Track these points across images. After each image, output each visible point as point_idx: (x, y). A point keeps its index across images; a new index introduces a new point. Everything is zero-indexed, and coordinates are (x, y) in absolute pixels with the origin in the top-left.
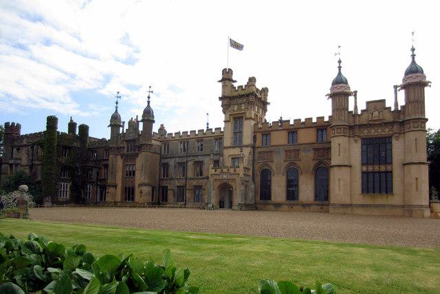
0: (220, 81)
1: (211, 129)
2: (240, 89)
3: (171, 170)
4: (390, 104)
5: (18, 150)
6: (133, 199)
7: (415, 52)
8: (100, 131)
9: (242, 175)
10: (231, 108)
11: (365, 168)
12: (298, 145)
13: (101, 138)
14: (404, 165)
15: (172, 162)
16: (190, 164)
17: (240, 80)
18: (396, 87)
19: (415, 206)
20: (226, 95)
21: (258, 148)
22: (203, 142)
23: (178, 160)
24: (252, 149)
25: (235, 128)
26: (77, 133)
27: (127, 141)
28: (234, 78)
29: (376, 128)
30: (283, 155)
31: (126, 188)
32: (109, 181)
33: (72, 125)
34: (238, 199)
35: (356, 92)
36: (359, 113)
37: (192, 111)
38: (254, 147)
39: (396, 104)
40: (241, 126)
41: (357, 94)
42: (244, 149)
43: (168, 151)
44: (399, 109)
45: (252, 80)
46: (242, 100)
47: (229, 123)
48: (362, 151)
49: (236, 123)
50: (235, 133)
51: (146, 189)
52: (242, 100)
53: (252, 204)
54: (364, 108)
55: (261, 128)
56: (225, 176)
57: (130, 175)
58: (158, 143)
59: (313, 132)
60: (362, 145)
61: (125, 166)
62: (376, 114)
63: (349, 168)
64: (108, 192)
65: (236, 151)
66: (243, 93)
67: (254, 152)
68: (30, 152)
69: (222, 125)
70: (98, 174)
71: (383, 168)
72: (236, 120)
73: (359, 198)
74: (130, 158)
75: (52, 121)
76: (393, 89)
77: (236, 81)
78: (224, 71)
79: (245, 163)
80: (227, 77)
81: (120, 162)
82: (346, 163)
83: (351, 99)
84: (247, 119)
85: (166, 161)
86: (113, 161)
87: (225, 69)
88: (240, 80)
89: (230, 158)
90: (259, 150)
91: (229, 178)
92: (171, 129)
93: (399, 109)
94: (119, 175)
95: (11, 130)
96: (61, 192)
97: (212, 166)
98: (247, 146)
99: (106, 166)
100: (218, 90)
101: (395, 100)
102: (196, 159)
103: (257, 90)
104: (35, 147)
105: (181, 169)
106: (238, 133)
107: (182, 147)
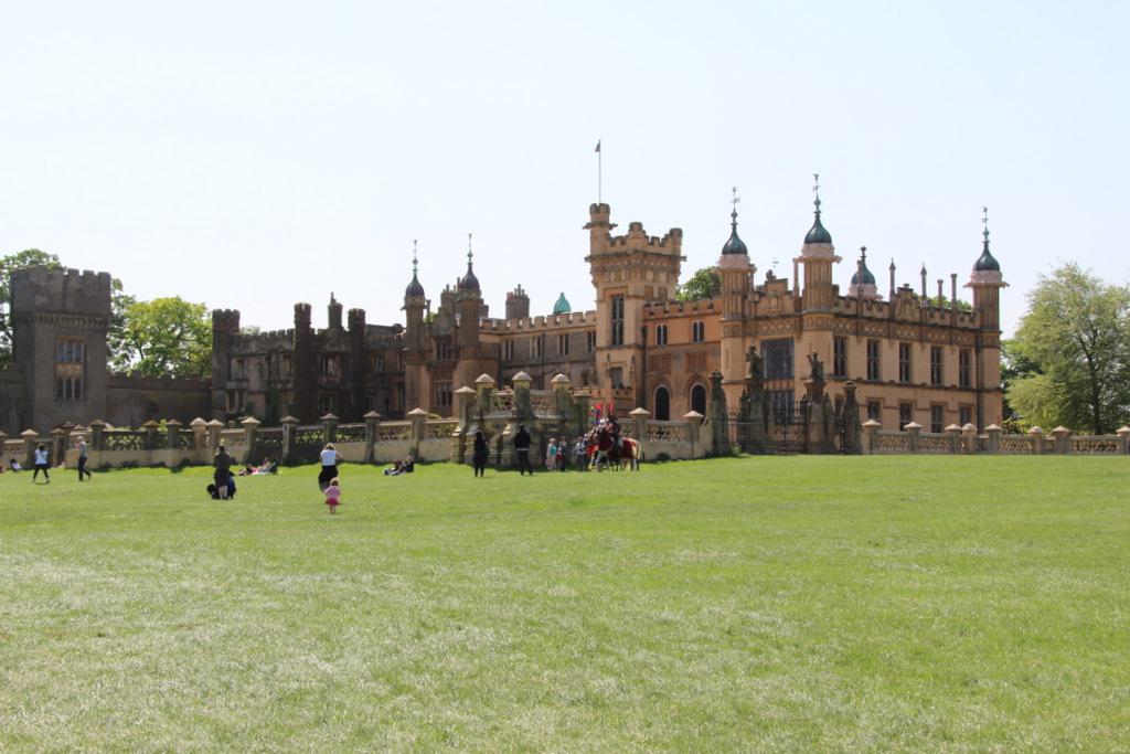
2: (618, 243)
5: (241, 362)
8: (387, 312)
9: (609, 400)
20: (596, 253)
21: (650, 348)
24: (638, 353)
27: (438, 339)
28: (612, 220)
30: (683, 360)
31: (60, 382)
33: (335, 310)
38: (642, 347)
40: (951, 321)
46: (627, 258)
47: (604, 305)
57: (444, 403)
58: (495, 340)
61: (434, 386)
66: (623, 249)
67: (644, 358)
68: (266, 367)
69: (593, 307)
70: (387, 401)
75: (303, 313)
80: (600, 214)
81: (425, 379)
86: (412, 378)
90: (651, 353)
99: (402, 386)
100: (583, 244)
104: (274, 358)
107: (536, 345)
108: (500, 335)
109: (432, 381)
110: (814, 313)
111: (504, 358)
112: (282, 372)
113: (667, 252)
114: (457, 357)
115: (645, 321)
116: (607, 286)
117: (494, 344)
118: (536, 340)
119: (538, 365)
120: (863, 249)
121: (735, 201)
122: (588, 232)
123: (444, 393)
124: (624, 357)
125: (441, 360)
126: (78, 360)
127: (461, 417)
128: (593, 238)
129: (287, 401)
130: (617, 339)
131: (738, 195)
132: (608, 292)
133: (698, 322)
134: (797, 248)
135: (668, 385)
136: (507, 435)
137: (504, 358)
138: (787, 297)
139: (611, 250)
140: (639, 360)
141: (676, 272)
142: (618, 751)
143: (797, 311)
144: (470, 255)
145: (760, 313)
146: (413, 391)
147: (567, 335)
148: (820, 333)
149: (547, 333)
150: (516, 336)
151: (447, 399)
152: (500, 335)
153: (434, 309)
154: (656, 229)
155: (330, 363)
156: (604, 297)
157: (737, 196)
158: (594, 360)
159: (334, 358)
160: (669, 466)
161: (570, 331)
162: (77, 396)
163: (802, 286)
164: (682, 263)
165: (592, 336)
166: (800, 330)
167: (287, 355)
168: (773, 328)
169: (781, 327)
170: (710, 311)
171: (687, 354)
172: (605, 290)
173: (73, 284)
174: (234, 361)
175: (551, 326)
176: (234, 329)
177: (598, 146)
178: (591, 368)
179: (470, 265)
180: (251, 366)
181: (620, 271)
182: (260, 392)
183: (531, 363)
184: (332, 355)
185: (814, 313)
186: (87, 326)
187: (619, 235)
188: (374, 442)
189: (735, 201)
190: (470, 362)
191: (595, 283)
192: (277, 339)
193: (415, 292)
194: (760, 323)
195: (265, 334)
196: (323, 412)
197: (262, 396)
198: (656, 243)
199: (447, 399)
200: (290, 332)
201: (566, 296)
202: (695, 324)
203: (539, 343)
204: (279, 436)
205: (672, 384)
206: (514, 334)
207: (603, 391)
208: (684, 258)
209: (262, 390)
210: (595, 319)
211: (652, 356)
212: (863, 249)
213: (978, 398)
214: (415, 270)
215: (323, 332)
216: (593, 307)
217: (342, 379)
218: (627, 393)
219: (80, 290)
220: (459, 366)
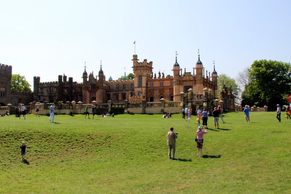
0: (132, 60)
2: (141, 64)
4: (192, 74)
8: (79, 80)
10: (137, 72)
13: (33, 82)
15: (112, 94)
16: (120, 95)
17: (141, 60)
18: (194, 68)
20: (135, 66)
23: (114, 92)
25: (139, 80)
26: (63, 81)
27: (91, 85)
30: (158, 91)
31: (5, 97)
35: (181, 69)
39: (194, 74)
40: (141, 79)
41: (182, 70)
42: (143, 88)
44: (195, 76)
45: (145, 60)
48: (184, 90)
50: (139, 82)
52: (143, 68)
56: (135, 100)
61: (90, 95)
65: (140, 89)
66: (142, 65)
67: (147, 90)
68: (49, 90)
76: (193, 69)
77: (138, 60)
78: (134, 56)
79: (144, 94)
80: (135, 58)
81: (88, 94)
83: (180, 71)
85: (109, 93)
89: (137, 92)
90: (149, 89)
91: (137, 100)
92: (115, 78)
93: (195, 76)
97: (130, 95)
98: (144, 87)
100: (131, 64)
102: (122, 92)
104: (51, 88)
105: (116, 96)
106: (140, 82)
108: (106, 84)
109: (90, 94)
110: (200, 80)
111: (107, 89)
112: (54, 91)
115: (147, 81)
120: (185, 69)
121: (199, 52)
122: (133, 61)
125: (92, 89)
126: (4, 87)
127: (181, 101)
128: (134, 63)
129: (56, 98)
130: (140, 86)
133: (162, 82)
134: (195, 66)
135: (154, 96)
136: (205, 106)
137: (107, 89)
138: (191, 76)
139: (139, 65)
142: (224, 193)
143: (194, 80)
144: (125, 73)
145: (184, 80)
146: (85, 97)
148: (201, 84)
150: (111, 85)
155: (65, 90)
156: (137, 76)
157: (177, 54)
158: (134, 90)
159: (66, 89)
160: (65, 115)
161: (126, 83)
162: (4, 96)
163: (195, 74)
166: (195, 84)
167: (55, 87)
168: (187, 83)
171: (169, 88)
172: (137, 74)
173: (3, 68)
174: (39, 89)
175: (121, 82)
177: (135, 42)
179: (101, 68)
180: (44, 90)
182: (47, 96)
183: (115, 90)
184: (66, 88)
185: (200, 80)
186: (6, 79)
187: (141, 62)
188: (145, 107)
189: (199, 52)
190: (102, 90)
192: (52, 84)
194: (184, 82)
196: (92, 100)
197: (48, 97)
200: (56, 82)
201: (112, 77)
202: (161, 82)
204: (107, 106)
205: (155, 96)
206: (110, 84)
207: (140, 97)
209: (48, 95)
211: (149, 90)
212: (185, 69)
215: (88, 81)
217: (68, 93)
219: (5, 70)
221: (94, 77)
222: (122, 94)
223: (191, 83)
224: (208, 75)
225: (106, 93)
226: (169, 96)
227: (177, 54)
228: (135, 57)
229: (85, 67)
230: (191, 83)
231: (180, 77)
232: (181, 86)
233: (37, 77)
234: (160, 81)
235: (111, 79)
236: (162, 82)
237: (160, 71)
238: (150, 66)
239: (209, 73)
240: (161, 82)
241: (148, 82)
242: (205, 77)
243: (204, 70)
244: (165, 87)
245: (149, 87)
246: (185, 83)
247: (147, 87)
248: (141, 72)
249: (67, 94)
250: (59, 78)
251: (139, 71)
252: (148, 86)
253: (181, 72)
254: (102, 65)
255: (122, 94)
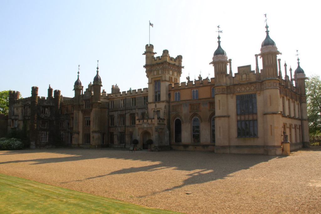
0: (144, 54)
1: (192, 82)
2: (158, 59)
3: (116, 120)
4: (253, 68)
5: (17, 109)
6: (89, 142)
7: (220, 40)
8: (68, 93)
9: (156, 125)
10: (152, 74)
11: (239, 118)
12: (199, 99)
14: (265, 114)
15: (116, 114)
16: (128, 116)
17: (158, 53)
18: (256, 56)
19: (271, 146)
20: (148, 64)
22: (135, 98)
24: (167, 104)
25: (156, 88)
26: (53, 95)
27: (86, 100)
29: (245, 87)
32: (74, 129)
33: (50, 90)
34: (93, 142)
35: (230, 60)
36: (233, 76)
37: (128, 76)
41: (232, 61)
43: (113, 107)
46: (161, 66)
47: (152, 85)
48: (237, 105)
49: (156, 84)
51: (96, 135)
52: (161, 66)
53: (167, 146)
54: (237, 72)
55: (173, 88)
56: (145, 126)
57: (87, 125)
58: (107, 101)
59: (208, 89)
60: (237, 100)
62: (244, 76)
63: (227, 118)
64: (74, 138)
66: (160, 61)
67: (169, 106)
69: (147, 86)
70: (68, 124)
71: (251, 118)
72: (155, 82)
73: (235, 142)
74: (86, 113)
75: (35, 90)
76: (255, 57)
77: (156, 53)
80: (149, 49)
81: (81, 115)
82: (225, 114)
84: (163, 81)
87: (147, 45)
88: (158, 53)
90: (173, 104)
94: (81, 125)
95: (13, 95)
96: (42, 137)
100: (143, 60)
101: (256, 65)
102: (131, 112)
103: (172, 59)
111: (110, 108)
113: (176, 65)
114: (92, 107)
115: (169, 91)
116: (152, 77)
117: (106, 102)
118: (123, 101)
119: (124, 110)
122: (145, 56)
123: (87, 121)
124: (162, 106)
125: (87, 108)
128: (147, 58)
130: (157, 98)
131: (220, 29)
132: (153, 80)
140: (167, 107)
141: (180, 73)
144: (98, 68)
147: (135, 98)
149: (127, 98)
150: (115, 99)
151: (89, 123)
152: (109, 99)
153: (84, 90)
154: (173, 54)
155: (46, 109)
156: (152, 81)
163: (261, 67)
164: (182, 69)
165: (146, 98)
169: (248, 89)
170: (201, 85)
172: (152, 79)
176: (16, 98)
178: (146, 111)
181: (159, 70)
182: (22, 120)
184: (47, 107)
190: (97, 109)
191: (148, 76)
192: (27, 101)
193: (78, 85)
194: (236, 87)
195: (24, 99)
198: (173, 60)
199: (89, 123)
203: (124, 101)
205: (183, 117)
208: (183, 67)
210: (147, 91)
211: (173, 106)
213: (301, 122)
214: (78, 76)
216: (147, 86)
218: (163, 121)
220: (93, 111)
221: (120, 91)
222: (131, 114)
223: (253, 88)
224: (289, 74)
225: (108, 114)
226: (208, 117)
227: (221, 32)
228: (149, 47)
229: (78, 73)
230: (253, 88)
231: (227, 78)
232: (229, 96)
233: (16, 92)
234: (192, 88)
235: (115, 90)
236: (195, 90)
237: (201, 74)
238: (177, 64)
239: (291, 70)
240: (194, 91)
241: (172, 93)
242: (283, 78)
243: (281, 62)
244: (201, 99)
245: (173, 102)
246: (238, 90)
247: (168, 102)
248: (158, 74)
249: (49, 116)
250: (215, 107)
251: (155, 73)
252: (172, 100)
253: (230, 65)
254: (99, 67)
255: (131, 114)
